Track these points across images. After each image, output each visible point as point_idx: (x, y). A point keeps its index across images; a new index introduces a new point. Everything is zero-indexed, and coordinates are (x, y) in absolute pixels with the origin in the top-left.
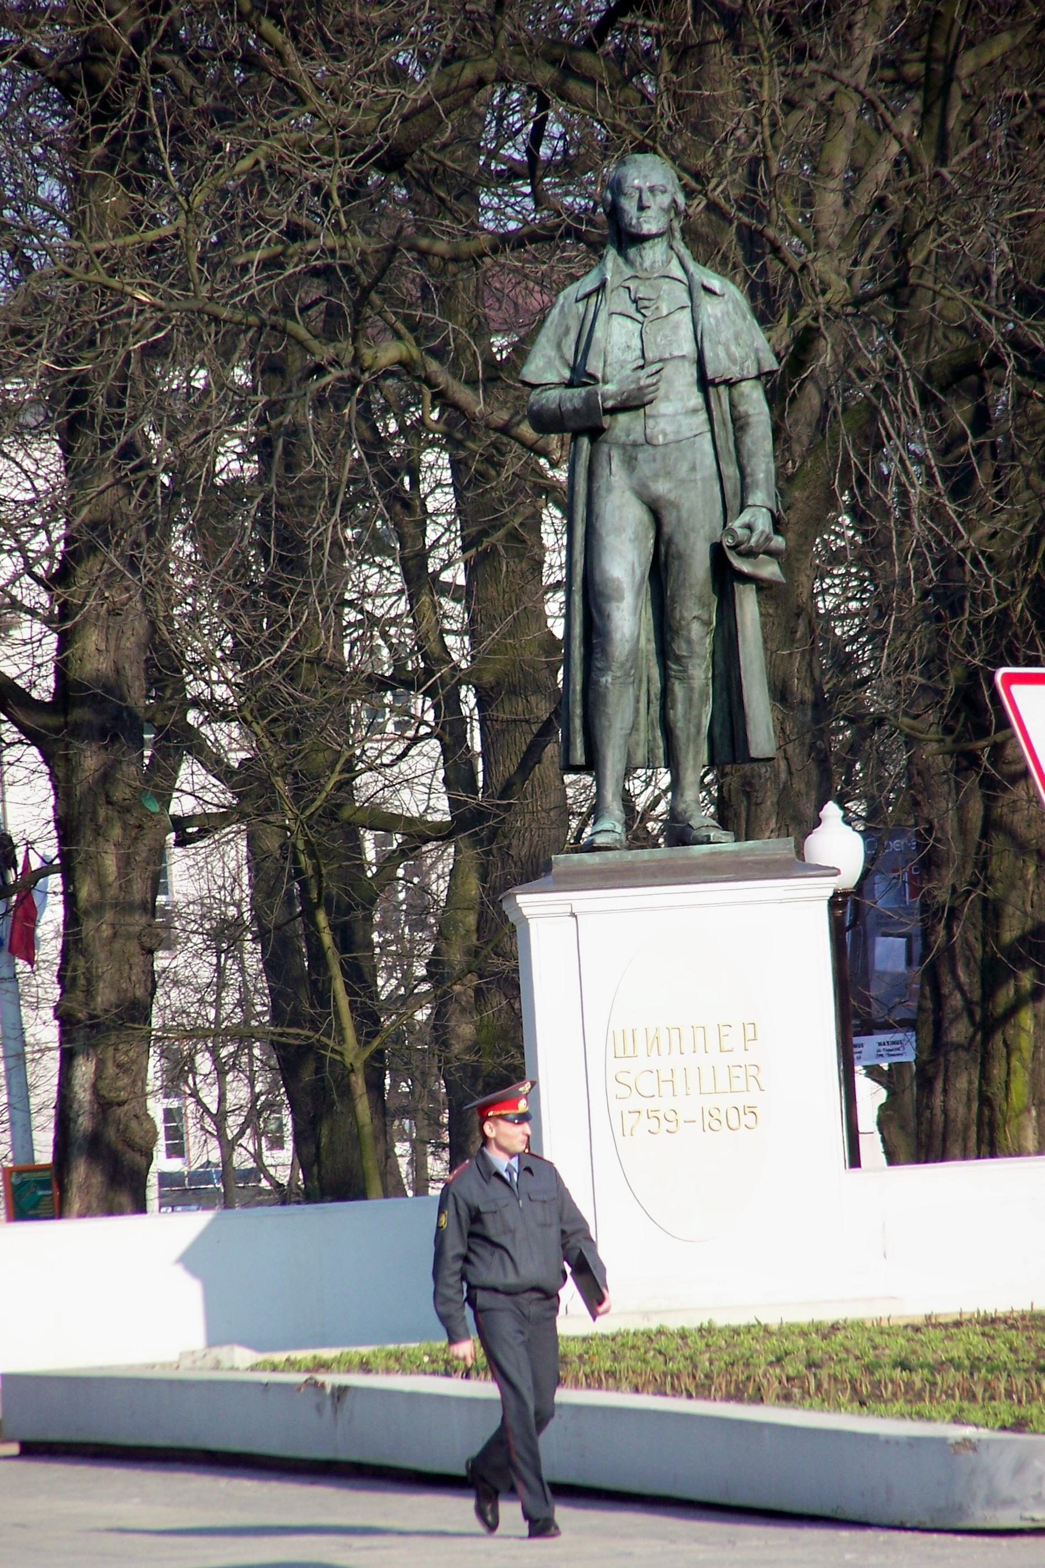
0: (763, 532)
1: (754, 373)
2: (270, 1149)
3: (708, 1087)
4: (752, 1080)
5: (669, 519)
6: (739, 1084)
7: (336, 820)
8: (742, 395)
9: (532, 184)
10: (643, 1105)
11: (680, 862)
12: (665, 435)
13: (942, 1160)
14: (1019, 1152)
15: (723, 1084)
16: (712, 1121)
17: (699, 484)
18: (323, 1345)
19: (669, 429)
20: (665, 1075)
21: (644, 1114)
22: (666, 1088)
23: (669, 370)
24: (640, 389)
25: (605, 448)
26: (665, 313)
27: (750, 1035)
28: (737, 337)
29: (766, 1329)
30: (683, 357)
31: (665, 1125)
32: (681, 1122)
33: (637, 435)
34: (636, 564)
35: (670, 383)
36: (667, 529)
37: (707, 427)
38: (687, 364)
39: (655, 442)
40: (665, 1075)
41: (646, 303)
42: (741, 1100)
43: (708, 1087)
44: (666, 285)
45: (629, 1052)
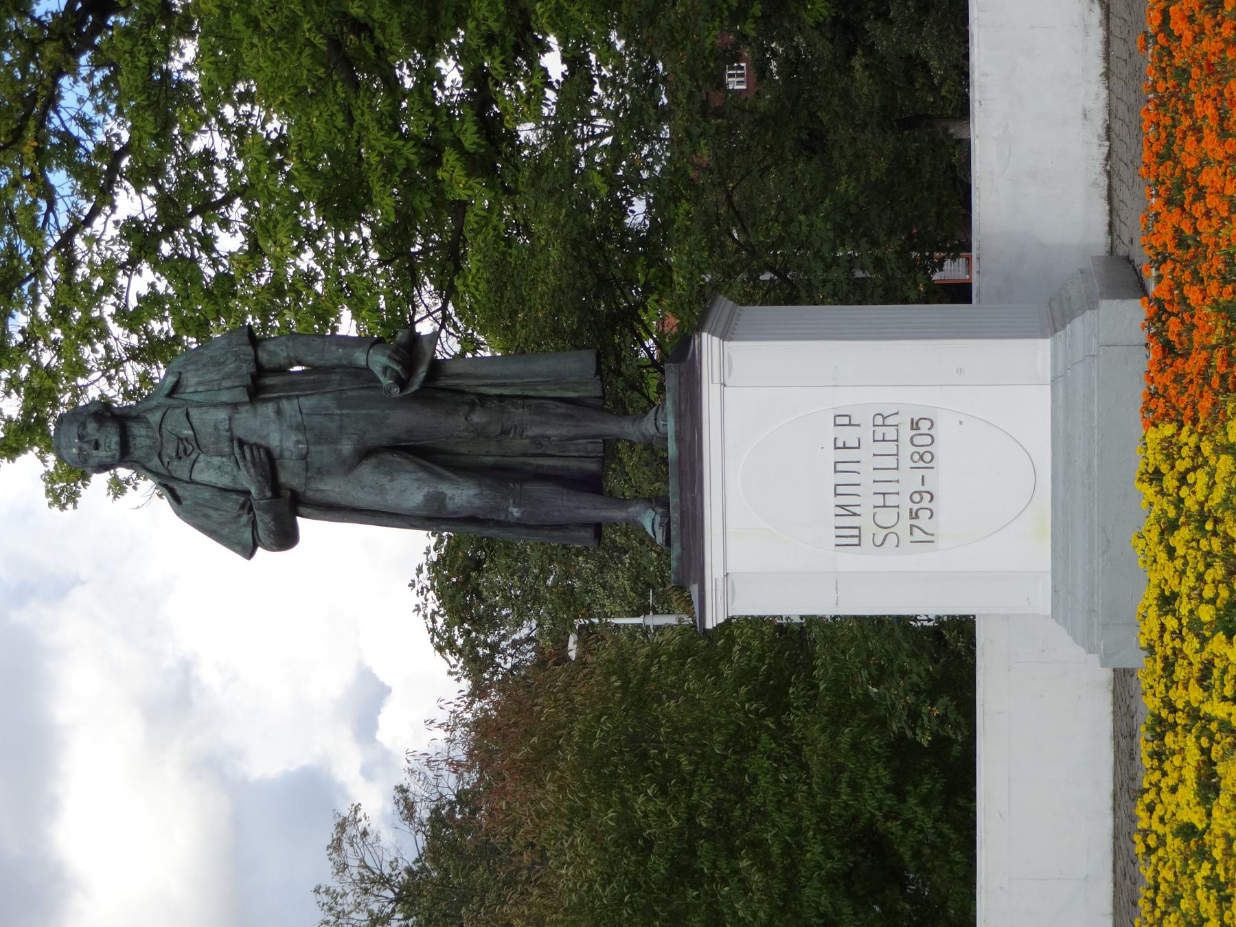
0: (390, 357)
2: (943, 653)
3: (891, 462)
4: (888, 422)
6: (891, 433)
9: (321, 173)
10: (906, 521)
12: (298, 442)
15: (891, 448)
16: (925, 460)
17: (344, 412)
19: (294, 438)
20: (879, 500)
21: (914, 522)
22: (891, 500)
23: (239, 432)
25: (310, 494)
26: (191, 432)
27: (845, 420)
29: (1109, 157)
30: (230, 419)
31: (925, 503)
32: (923, 489)
34: (413, 476)
36: (385, 442)
37: (239, 487)
39: (304, 451)
40: (879, 500)
42: (906, 433)
43: (891, 462)
44: (167, 427)
45: (856, 532)
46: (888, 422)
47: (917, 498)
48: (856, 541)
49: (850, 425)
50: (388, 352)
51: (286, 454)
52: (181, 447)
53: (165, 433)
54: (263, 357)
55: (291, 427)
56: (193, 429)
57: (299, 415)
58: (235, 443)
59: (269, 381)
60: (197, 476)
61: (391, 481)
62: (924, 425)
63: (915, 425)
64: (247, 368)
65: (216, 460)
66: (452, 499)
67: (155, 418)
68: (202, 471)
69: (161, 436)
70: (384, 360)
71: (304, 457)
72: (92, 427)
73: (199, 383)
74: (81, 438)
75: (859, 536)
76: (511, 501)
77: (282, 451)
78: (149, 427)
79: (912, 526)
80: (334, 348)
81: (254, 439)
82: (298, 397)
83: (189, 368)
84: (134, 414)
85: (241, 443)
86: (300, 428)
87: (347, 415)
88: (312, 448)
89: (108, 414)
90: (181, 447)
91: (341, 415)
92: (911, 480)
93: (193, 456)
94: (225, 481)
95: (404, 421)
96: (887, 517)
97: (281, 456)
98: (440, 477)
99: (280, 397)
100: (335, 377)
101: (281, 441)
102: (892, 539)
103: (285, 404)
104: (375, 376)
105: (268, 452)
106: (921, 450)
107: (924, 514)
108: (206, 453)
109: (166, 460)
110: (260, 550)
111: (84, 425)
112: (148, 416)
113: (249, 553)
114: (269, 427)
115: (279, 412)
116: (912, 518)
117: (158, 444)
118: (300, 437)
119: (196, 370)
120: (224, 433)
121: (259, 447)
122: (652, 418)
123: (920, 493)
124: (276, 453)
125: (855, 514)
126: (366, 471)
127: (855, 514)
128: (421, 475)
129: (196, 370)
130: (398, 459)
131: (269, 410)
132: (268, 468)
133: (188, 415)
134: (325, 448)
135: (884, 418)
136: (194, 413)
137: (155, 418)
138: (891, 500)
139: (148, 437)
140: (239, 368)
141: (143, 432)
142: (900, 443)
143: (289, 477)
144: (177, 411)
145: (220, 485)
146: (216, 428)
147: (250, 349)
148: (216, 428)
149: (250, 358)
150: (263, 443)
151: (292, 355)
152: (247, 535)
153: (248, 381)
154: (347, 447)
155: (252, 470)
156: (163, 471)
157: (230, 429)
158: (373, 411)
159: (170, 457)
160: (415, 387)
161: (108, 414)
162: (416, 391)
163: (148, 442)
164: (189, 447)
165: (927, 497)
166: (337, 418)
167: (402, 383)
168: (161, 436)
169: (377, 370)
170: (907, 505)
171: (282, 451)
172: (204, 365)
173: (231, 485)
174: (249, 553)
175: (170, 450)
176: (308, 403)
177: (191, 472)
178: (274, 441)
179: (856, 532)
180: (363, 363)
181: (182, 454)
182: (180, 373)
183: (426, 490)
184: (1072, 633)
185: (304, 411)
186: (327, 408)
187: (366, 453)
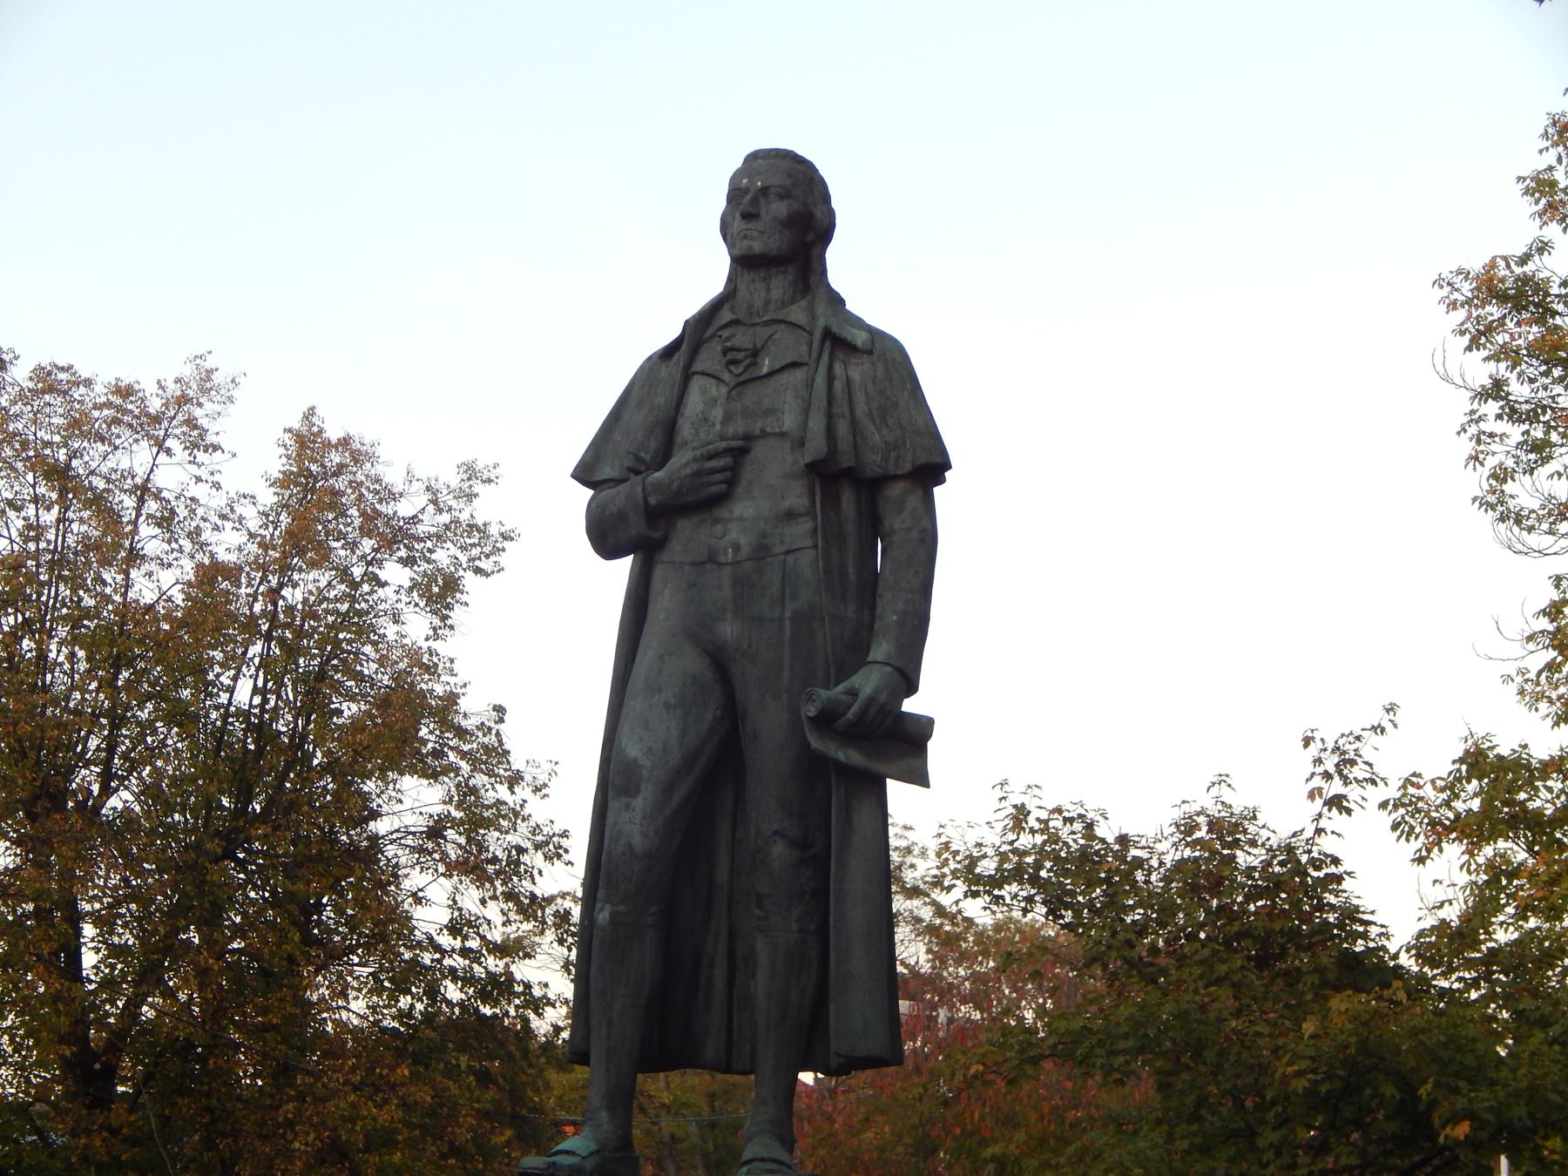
0: (871, 699)
17: (788, 624)
23: (760, 450)
26: (765, 370)
30: (783, 435)
39: (722, 559)
50: (882, 698)
51: (719, 529)
52: (740, 356)
53: (769, 330)
54: (896, 490)
55: (764, 535)
56: (771, 374)
57: (784, 548)
58: (740, 443)
59: (847, 498)
60: (696, 384)
61: (667, 705)
64: (873, 462)
65: (717, 413)
66: (628, 807)
67: (797, 313)
68: (703, 391)
69: (767, 323)
70: (867, 690)
71: (712, 558)
72: (780, 208)
73: (849, 383)
74: (764, 191)
76: (622, 908)
78: (784, 304)
80: (900, 606)
81: (747, 473)
83: (880, 366)
84: (813, 280)
86: (761, 551)
88: (727, 572)
90: (740, 356)
91: (781, 620)
93: (726, 377)
94: (685, 429)
95: (769, 724)
97: (716, 521)
98: (668, 789)
99: (815, 518)
100: (851, 610)
101: (741, 519)
103: (805, 525)
104: (847, 677)
108: (729, 396)
109: (725, 333)
110: (590, 493)
111: (785, 195)
112: (803, 303)
113: (583, 474)
114: (770, 495)
115: (791, 515)
117: (757, 320)
118: (745, 552)
120: (759, 425)
121: (732, 483)
122: (766, 1154)
124: (723, 513)
126: (692, 662)
130: (709, 716)
131: (796, 497)
132: (692, 498)
133: (794, 365)
134: (727, 593)
136: (799, 375)
137: (797, 313)
139: (767, 303)
141: (776, 294)
143: (688, 537)
144: (804, 348)
145: (680, 421)
146: (769, 412)
147: (907, 467)
148: (769, 412)
149: (891, 470)
150: (740, 490)
151: (895, 538)
152: (607, 471)
153: (846, 461)
154: (728, 630)
155: (688, 471)
156: (716, 324)
158: (786, 674)
159: (727, 339)
160: (815, 742)
161: (810, 238)
162: (808, 744)
163: (759, 303)
164: (744, 369)
167: (826, 720)
168: (767, 323)
169: (856, 680)
173: (678, 440)
174: (583, 474)
175: (742, 338)
176: (805, 563)
177: (703, 373)
180: (871, 658)
181: (730, 356)
182: (870, 352)
185: (790, 558)
187: (719, 661)
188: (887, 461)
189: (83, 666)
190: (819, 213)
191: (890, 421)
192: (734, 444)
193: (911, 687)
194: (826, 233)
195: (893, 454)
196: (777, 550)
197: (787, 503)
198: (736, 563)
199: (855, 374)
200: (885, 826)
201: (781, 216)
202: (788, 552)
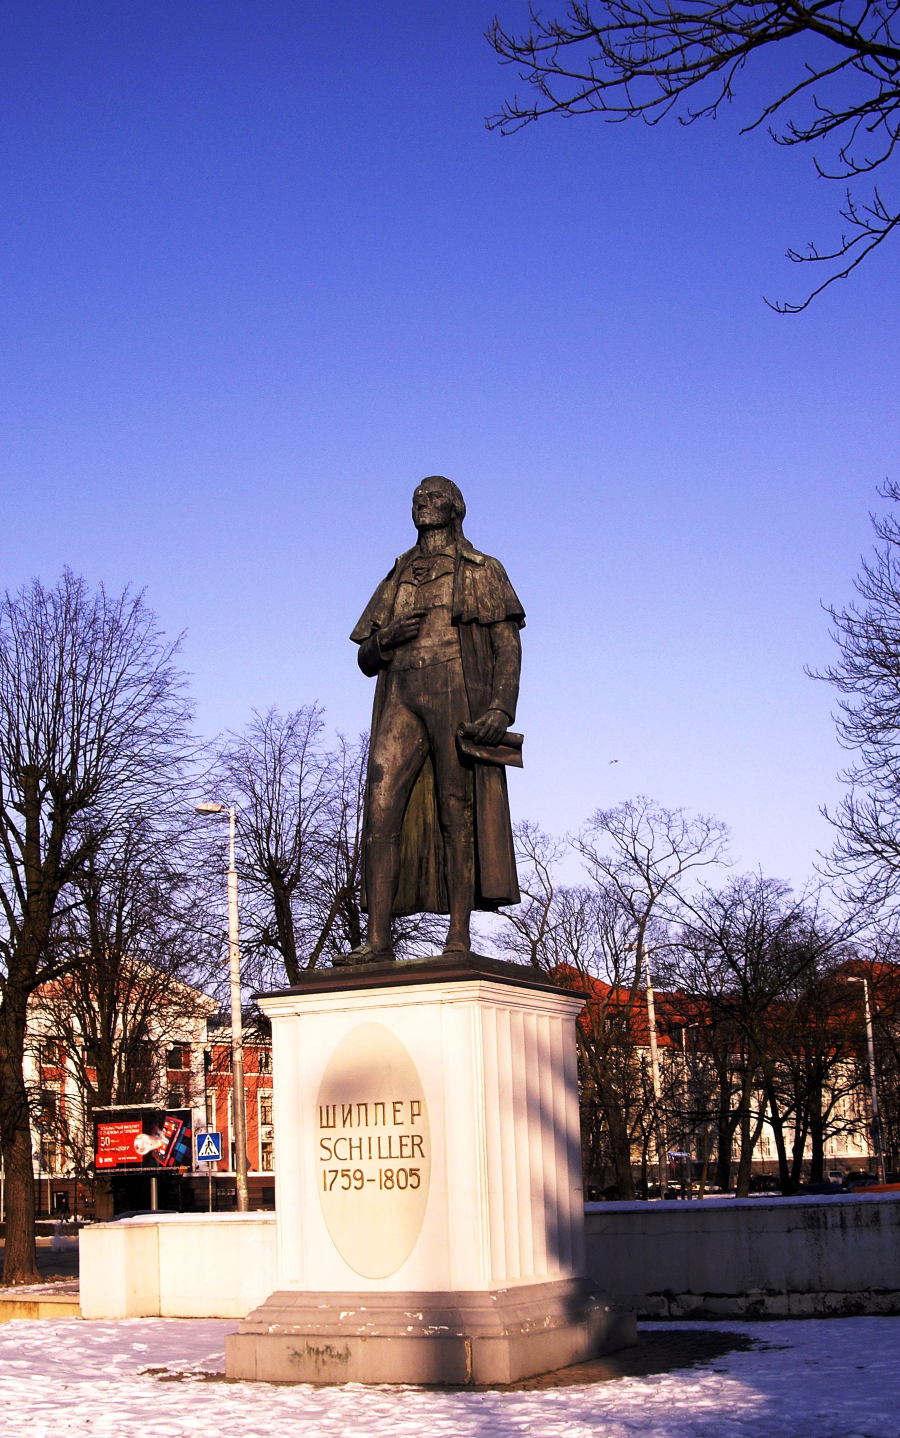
1: (503, 616)
3: (385, 1153)
4: (416, 1147)
5: (430, 720)
6: (407, 1151)
7: (155, 932)
8: (496, 633)
10: (340, 1166)
11: (79, 847)
12: (424, 660)
13: (78, 1250)
14: (78, 1240)
15: (396, 1152)
18: (154, 1362)
20: (355, 1143)
22: (356, 1152)
23: (431, 617)
24: (401, 627)
28: (491, 593)
30: (443, 606)
31: (355, 1183)
33: (406, 664)
34: (398, 755)
35: (432, 625)
38: (445, 611)
40: (355, 1143)
41: (420, 571)
42: (408, 1164)
43: (385, 1153)
45: (331, 1124)
46: (416, 1147)
47: (358, 1175)
48: (325, 1124)
49: (413, 1115)
51: (415, 652)
54: (500, 628)
56: (436, 579)
60: (403, 587)
62: (413, 1180)
63: (414, 1172)
65: (412, 599)
66: (378, 786)
68: (405, 590)
73: (474, 580)
75: (328, 1127)
77: (417, 649)
79: (337, 1171)
82: (461, 657)
83: (489, 572)
85: (422, 616)
87: (447, 697)
89: (453, 515)
91: (447, 692)
92: (372, 1168)
93: (416, 582)
96: (343, 1149)
97: (413, 649)
98: (396, 777)
101: (425, 647)
102: (326, 1154)
103: (456, 647)
105: (415, 638)
106: (395, 1178)
107: (345, 1182)
108: (417, 592)
114: (437, 640)
115: (449, 643)
116: (343, 1171)
119: (486, 577)
123: (362, 1178)
125: (344, 1122)
127: (344, 1122)
128: (400, 761)
129: (486, 577)
131: (451, 634)
133: (448, 573)
134: (420, 682)
135: (418, 1145)
136: (449, 579)
137: (449, 551)
138: (356, 1152)
140: (487, 610)
142: (399, 1159)
157: (435, 607)
162: (461, 749)
165: (359, 1184)
166: (445, 690)
170: (352, 1165)
171: (417, 649)
172: (490, 583)
177: (406, 582)
178: (425, 642)
179: (331, 1124)
183: (386, 766)
184: (258, 1311)
186: (453, 680)
188: (494, 615)
189: (324, 869)
190: (457, 504)
191: (495, 596)
192: (419, 612)
193: (512, 721)
194: (461, 515)
195: (497, 611)
196: (443, 660)
197: (447, 638)
198: (424, 668)
199: (477, 576)
200: (469, 932)
201: (440, 510)
202: (448, 661)
